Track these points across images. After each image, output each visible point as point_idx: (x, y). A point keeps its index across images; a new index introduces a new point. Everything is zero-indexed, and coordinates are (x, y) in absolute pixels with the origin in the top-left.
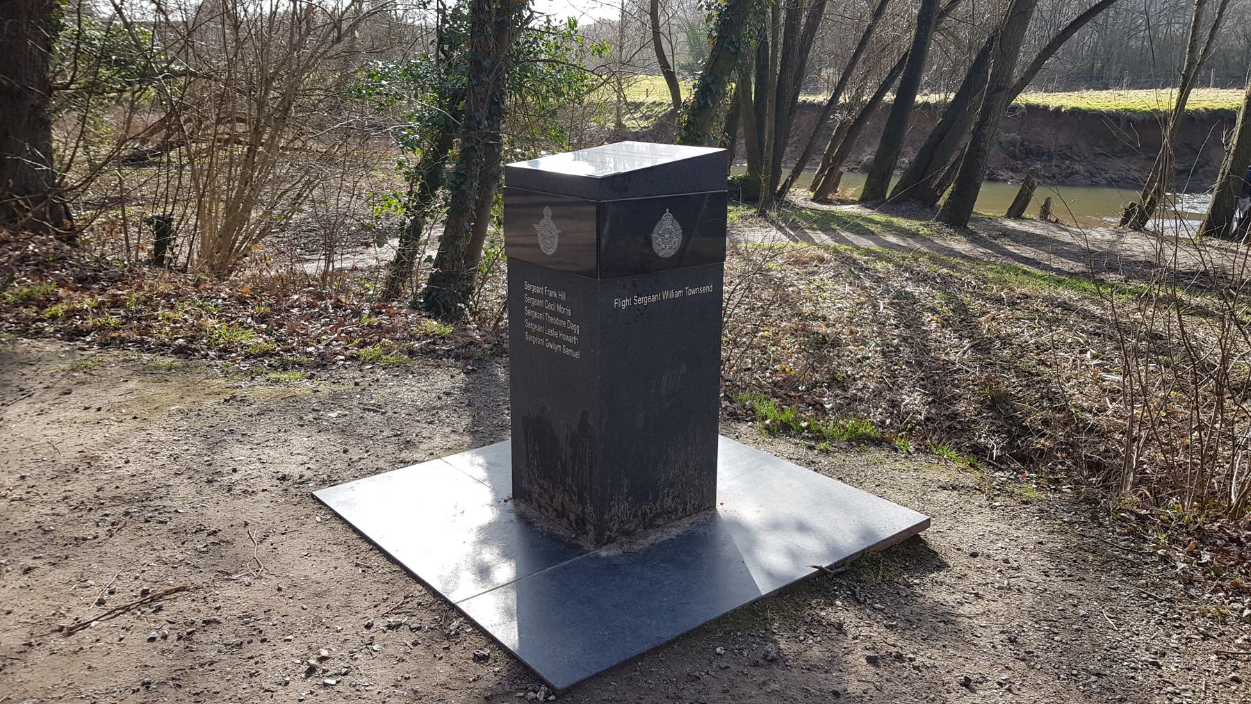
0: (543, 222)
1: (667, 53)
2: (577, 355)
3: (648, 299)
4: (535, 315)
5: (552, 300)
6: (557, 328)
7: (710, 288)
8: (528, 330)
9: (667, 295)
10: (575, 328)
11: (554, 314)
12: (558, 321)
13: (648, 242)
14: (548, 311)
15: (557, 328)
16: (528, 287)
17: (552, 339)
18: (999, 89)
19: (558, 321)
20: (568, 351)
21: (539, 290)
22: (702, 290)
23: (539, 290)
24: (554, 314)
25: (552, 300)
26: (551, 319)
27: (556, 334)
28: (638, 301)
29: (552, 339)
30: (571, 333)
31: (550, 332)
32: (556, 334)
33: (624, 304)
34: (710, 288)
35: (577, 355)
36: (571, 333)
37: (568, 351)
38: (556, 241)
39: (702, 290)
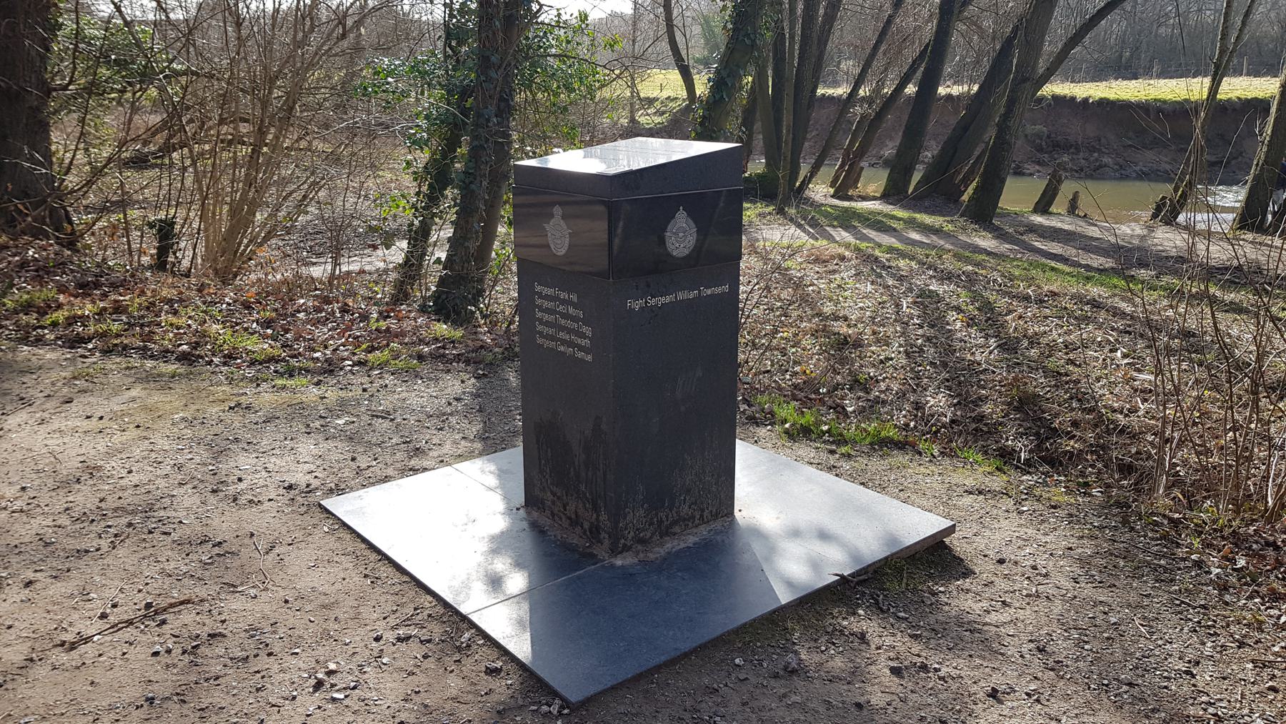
2: (589, 358)
3: (662, 300)
5: (563, 302)
6: (569, 331)
7: (726, 288)
10: (587, 331)
12: (569, 324)
13: (662, 241)
15: (569, 331)
16: (538, 289)
17: (563, 342)
18: (1025, 80)
19: (569, 324)
20: (580, 355)
21: (549, 291)
22: (718, 290)
23: (549, 291)
24: (566, 316)
25: (563, 302)
26: (563, 322)
28: (652, 302)
29: (563, 342)
30: (583, 336)
31: (562, 335)
33: (637, 305)
34: (726, 288)
35: (589, 358)
36: (583, 336)
37: (580, 355)
39: (718, 290)
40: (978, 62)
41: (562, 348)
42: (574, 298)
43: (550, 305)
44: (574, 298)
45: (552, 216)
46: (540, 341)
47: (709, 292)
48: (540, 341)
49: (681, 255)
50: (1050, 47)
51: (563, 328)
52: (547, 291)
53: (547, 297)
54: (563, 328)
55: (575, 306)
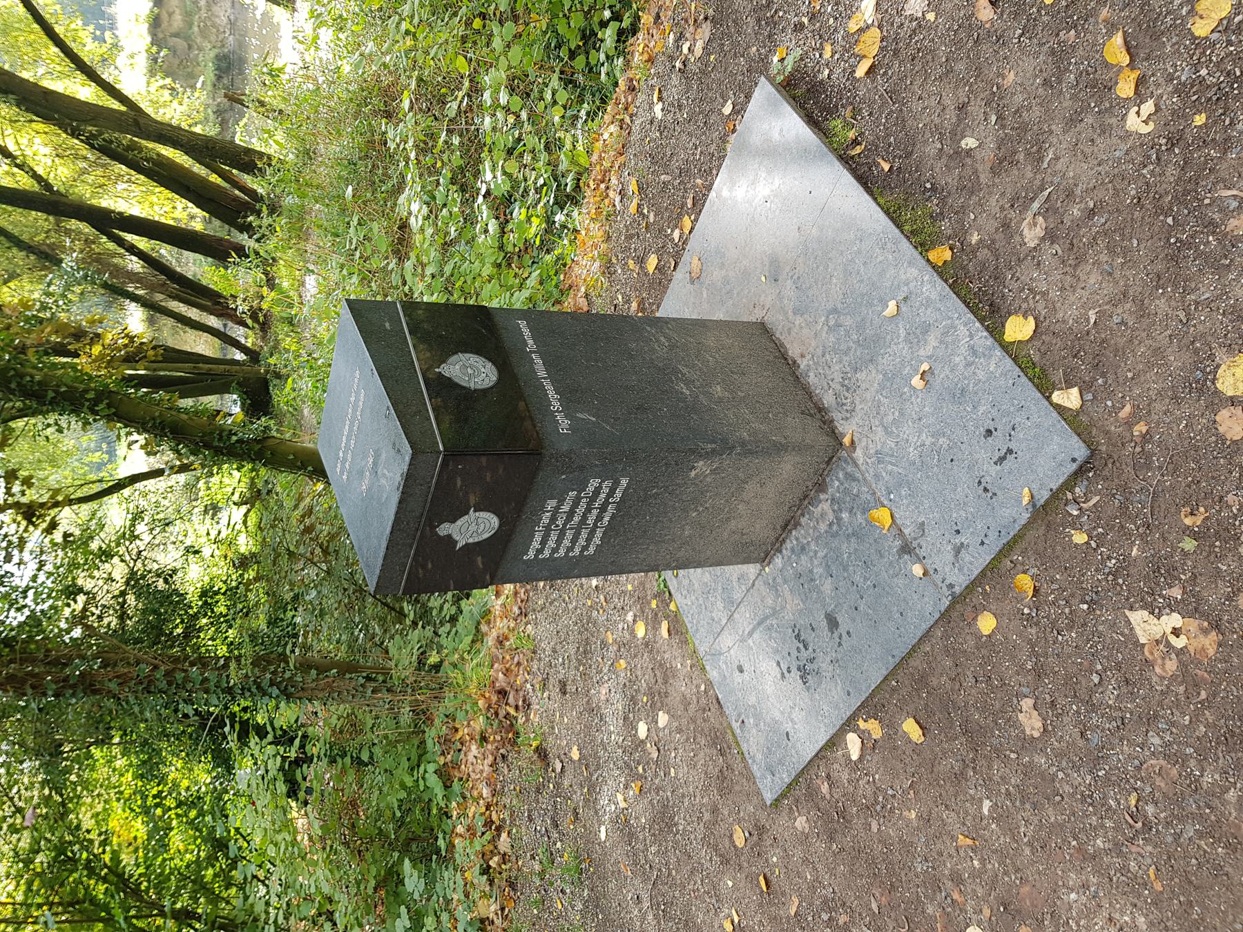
0: (456, 537)
1: (96, 488)
2: (624, 482)
3: (551, 393)
4: (566, 542)
5: (553, 519)
6: (589, 510)
7: (522, 324)
8: (582, 552)
9: (542, 373)
10: (593, 483)
11: (571, 514)
12: (580, 510)
13: (485, 391)
14: (565, 525)
15: (589, 510)
16: (531, 554)
17: (599, 518)
18: (136, 123)
19: (580, 510)
20: (618, 494)
21: (538, 538)
22: (526, 332)
23: (538, 538)
24: (571, 514)
25: (553, 519)
26: (576, 519)
27: (595, 512)
28: (556, 405)
29: (599, 518)
30: (597, 491)
31: (590, 521)
32: (595, 512)
33: (564, 423)
34: (522, 324)
35: (624, 482)
36: (597, 491)
37: (618, 494)
38: (482, 514)
39: (526, 332)
40: (104, 166)
41: (606, 519)
42: (552, 504)
43: (554, 537)
44: (573, 494)
45: (449, 536)
46: (592, 550)
47: (530, 342)
48: (592, 550)
49: (496, 373)
50: (85, 92)
51: (585, 517)
52: (536, 544)
53: (544, 542)
54: (585, 517)
55: (561, 502)
